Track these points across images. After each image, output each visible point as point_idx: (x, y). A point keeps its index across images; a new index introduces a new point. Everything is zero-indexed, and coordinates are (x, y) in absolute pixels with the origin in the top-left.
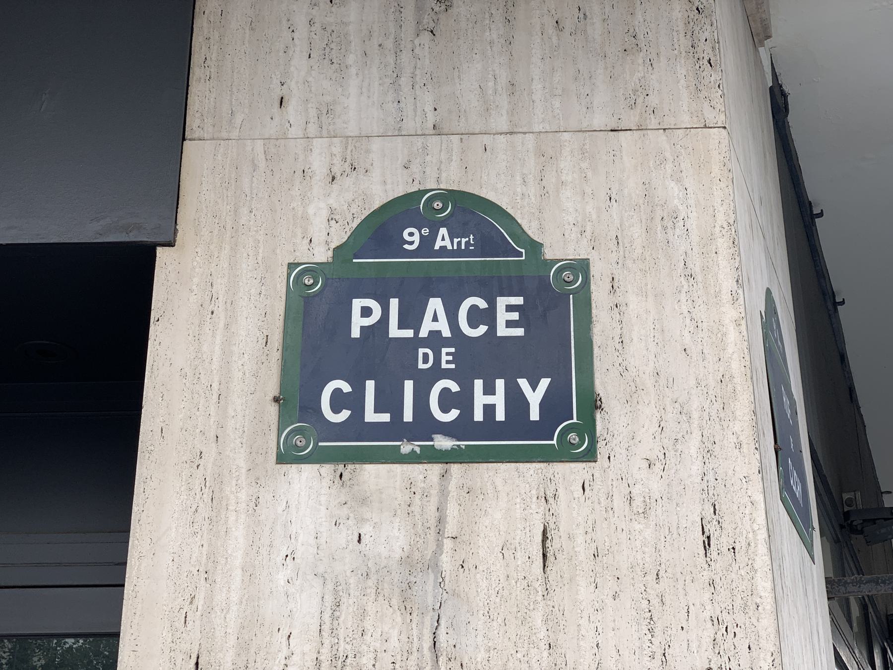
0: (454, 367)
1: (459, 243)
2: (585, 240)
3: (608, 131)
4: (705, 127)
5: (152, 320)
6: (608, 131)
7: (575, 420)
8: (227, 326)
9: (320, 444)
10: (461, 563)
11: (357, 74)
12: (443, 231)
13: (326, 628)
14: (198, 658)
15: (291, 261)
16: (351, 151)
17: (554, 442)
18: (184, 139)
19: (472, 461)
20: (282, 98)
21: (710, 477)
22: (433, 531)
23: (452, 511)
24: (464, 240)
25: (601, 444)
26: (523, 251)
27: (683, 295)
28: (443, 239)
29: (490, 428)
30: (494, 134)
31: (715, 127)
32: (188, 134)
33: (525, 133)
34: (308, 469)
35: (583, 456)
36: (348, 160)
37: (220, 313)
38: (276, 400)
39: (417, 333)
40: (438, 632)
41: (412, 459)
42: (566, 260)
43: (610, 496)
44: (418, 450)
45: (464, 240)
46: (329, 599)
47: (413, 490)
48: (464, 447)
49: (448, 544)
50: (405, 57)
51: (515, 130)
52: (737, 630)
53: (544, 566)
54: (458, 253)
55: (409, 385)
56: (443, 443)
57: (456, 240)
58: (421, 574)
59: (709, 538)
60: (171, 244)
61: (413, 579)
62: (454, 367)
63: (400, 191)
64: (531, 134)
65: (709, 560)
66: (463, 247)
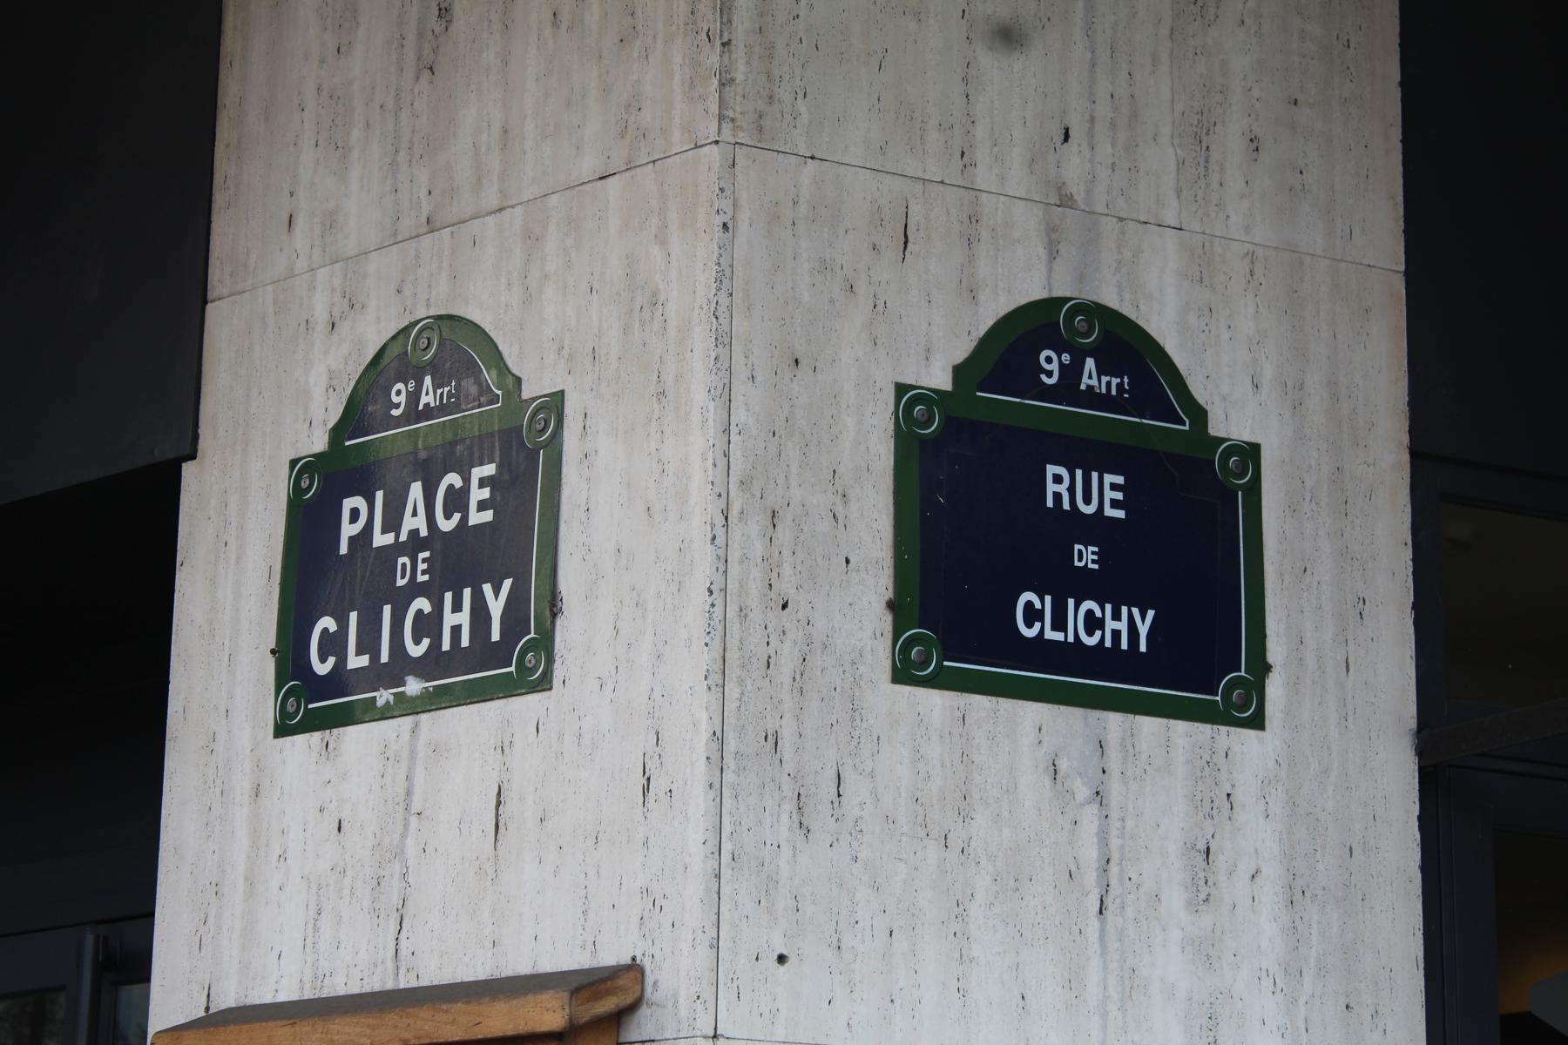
0: (1123, 648)
1: (1109, 384)
2: (563, 361)
3: (596, 180)
4: (697, 147)
5: (178, 565)
6: (596, 180)
7: (532, 635)
8: (238, 560)
9: (310, 706)
10: (423, 846)
11: (359, 159)
12: (1090, 363)
13: (309, 941)
14: (209, 989)
15: (293, 457)
16: (351, 279)
17: (512, 669)
18: (206, 302)
19: (439, 707)
20: (291, 216)
21: (657, 695)
22: (401, 809)
23: (419, 779)
24: (1115, 381)
25: (557, 665)
26: (499, 392)
27: (654, 423)
28: (1090, 376)
29: (455, 660)
30: (484, 216)
31: (706, 145)
32: (210, 297)
33: (513, 207)
34: (300, 739)
35: (539, 684)
36: (347, 296)
37: (233, 546)
38: (273, 652)
39: (397, 537)
40: (400, 937)
41: (386, 714)
42: (922, 388)
43: (561, 736)
44: (391, 698)
45: (1115, 381)
46: (313, 907)
47: (387, 755)
48: (431, 689)
49: (413, 820)
50: (405, 115)
51: (505, 204)
52: (664, 902)
53: (496, 839)
54: (443, 409)
55: (387, 609)
56: (413, 686)
57: (1105, 379)
58: (389, 865)
59: (649, 779)
60: (192, 456)
61: (382, 873)
62: (1123, 648)
63: (1037, 293)
64: (520, 206)
65: (646, 810)
66: (1114, 392)
